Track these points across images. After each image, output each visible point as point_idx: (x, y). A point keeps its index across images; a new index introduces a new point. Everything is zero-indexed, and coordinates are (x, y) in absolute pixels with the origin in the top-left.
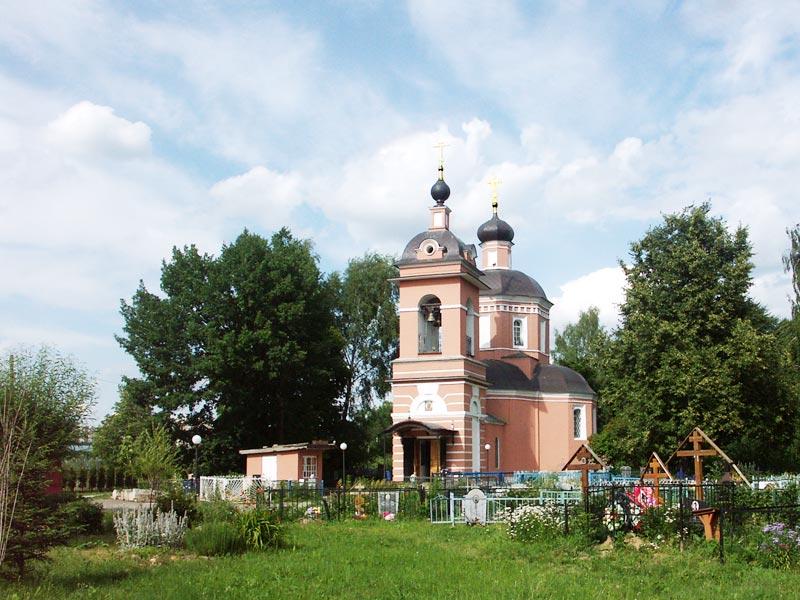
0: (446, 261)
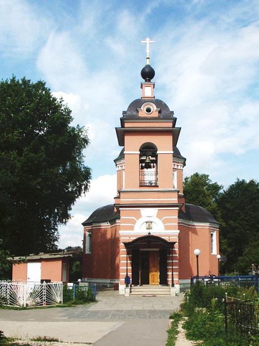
0: (162, 119)
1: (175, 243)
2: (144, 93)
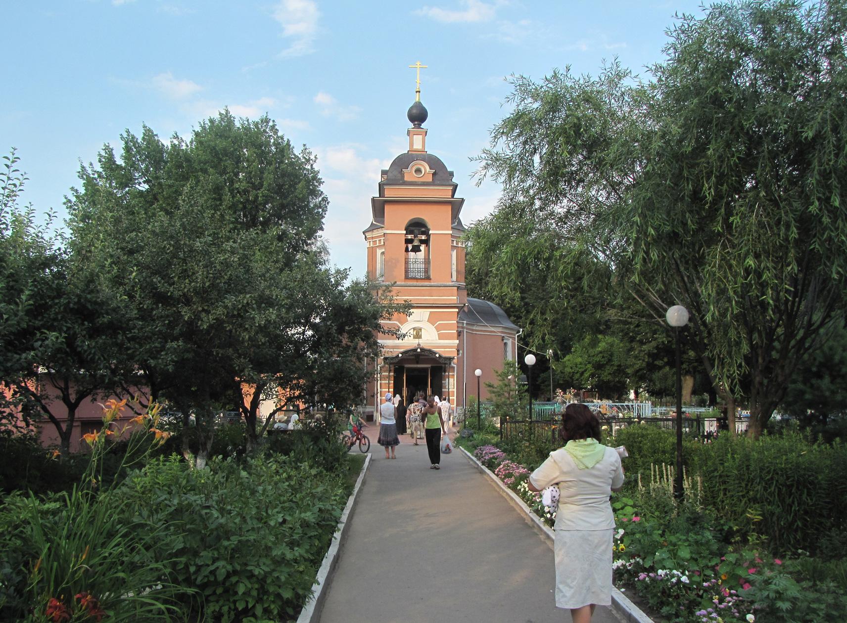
1: (453, 358)
2: (411, 144)
